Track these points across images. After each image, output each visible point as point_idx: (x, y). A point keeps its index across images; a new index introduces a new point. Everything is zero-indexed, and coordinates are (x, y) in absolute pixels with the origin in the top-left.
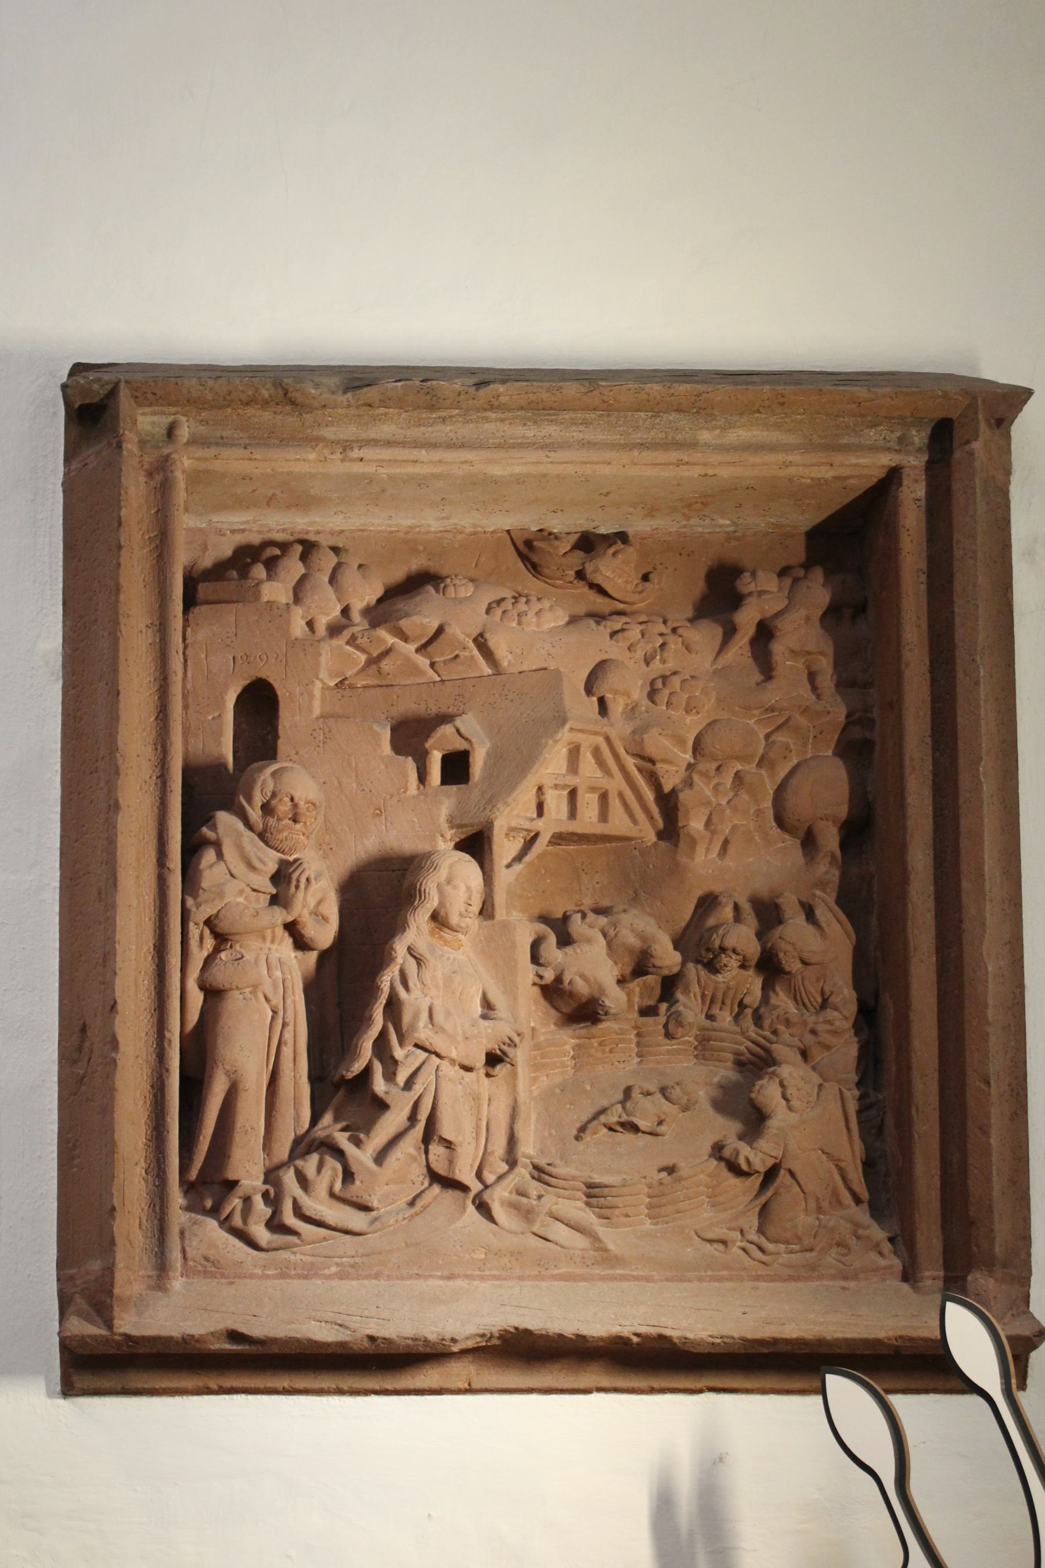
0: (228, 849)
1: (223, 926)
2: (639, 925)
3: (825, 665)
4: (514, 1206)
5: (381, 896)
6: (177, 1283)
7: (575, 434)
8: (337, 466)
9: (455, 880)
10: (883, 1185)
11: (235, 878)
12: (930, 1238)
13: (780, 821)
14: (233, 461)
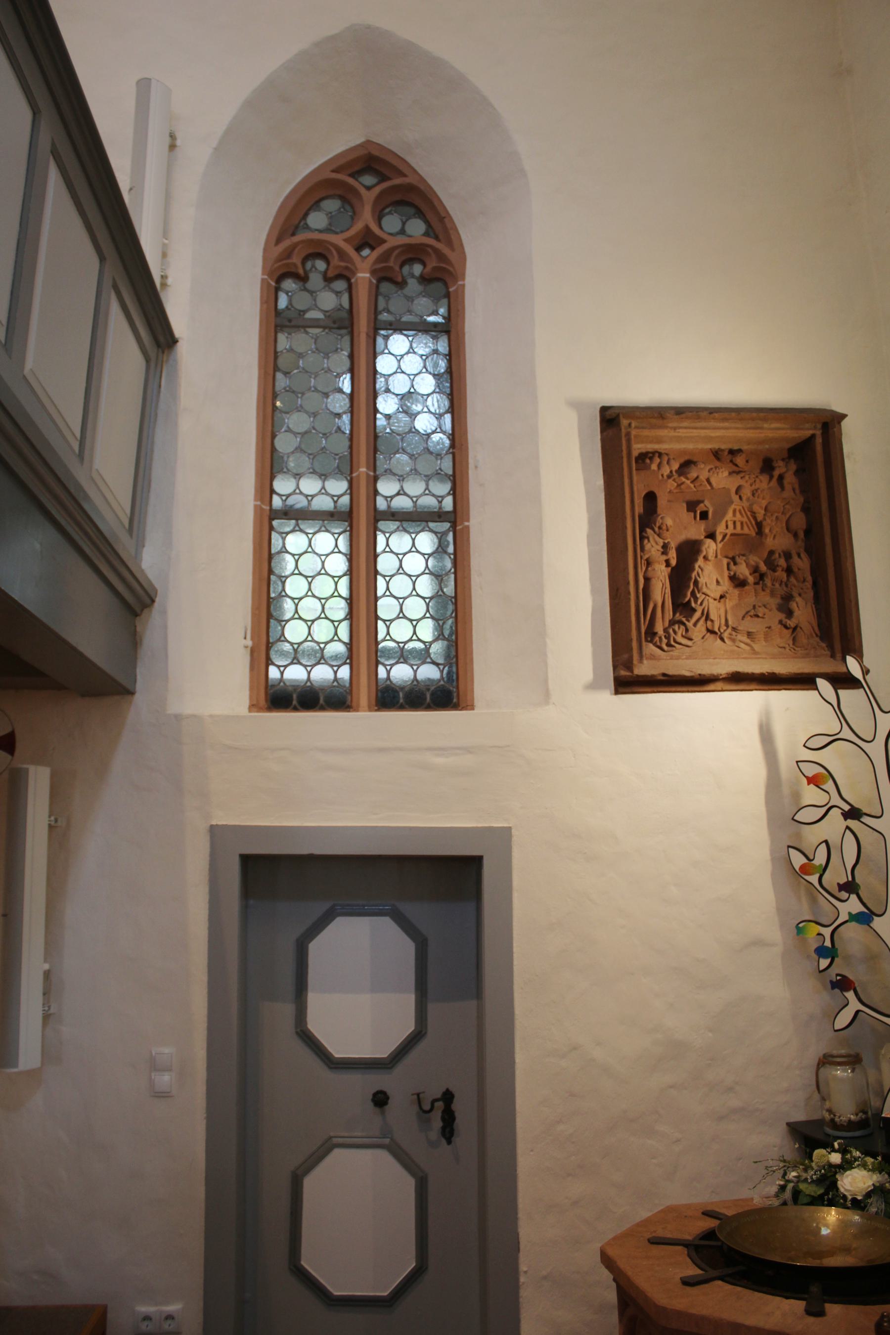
0: (651, 539)
1: (651, 560)
2: (754, 559)
3: (797, 486)
4: (730, 639)
5: (689, 552)
6: (645, 662)
7: (733, 425)
8: (672, 433)
9: (710, 547)
10: (824, 633)
11: (653, 547)
12: (838, 646)
13: (788, 529)
14: (646, 433)
